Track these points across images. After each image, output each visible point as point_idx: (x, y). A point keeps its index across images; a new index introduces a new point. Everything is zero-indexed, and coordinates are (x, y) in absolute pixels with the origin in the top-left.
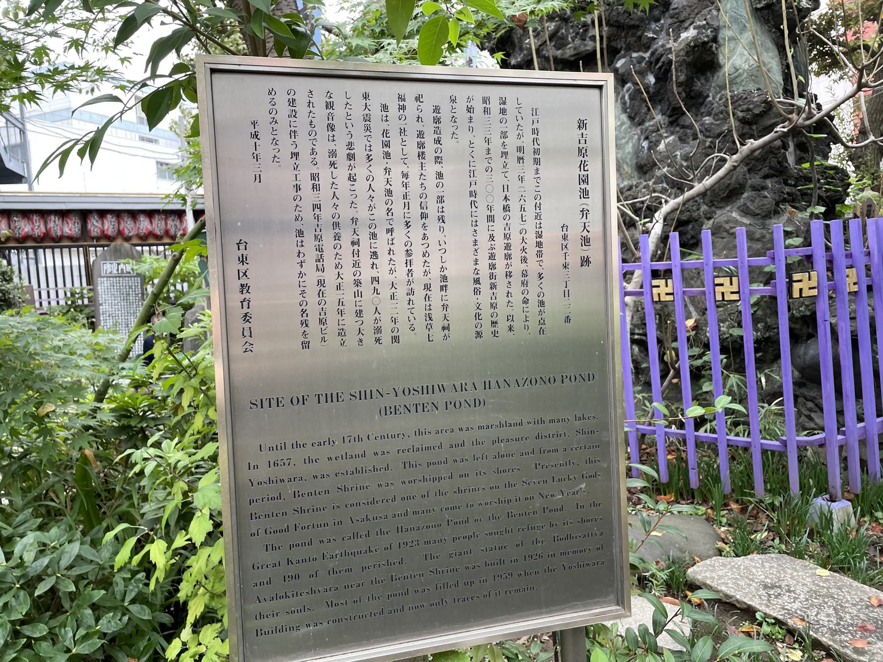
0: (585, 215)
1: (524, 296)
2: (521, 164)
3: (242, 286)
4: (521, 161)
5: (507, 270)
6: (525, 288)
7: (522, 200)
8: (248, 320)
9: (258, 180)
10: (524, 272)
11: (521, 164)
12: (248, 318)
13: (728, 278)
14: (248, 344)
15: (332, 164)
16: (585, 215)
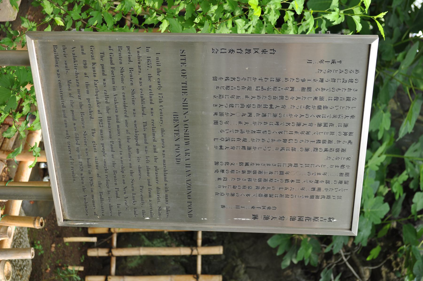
3: (250, 50)
8: (231, 52)
9: (309, 62)
12: (231, 52)
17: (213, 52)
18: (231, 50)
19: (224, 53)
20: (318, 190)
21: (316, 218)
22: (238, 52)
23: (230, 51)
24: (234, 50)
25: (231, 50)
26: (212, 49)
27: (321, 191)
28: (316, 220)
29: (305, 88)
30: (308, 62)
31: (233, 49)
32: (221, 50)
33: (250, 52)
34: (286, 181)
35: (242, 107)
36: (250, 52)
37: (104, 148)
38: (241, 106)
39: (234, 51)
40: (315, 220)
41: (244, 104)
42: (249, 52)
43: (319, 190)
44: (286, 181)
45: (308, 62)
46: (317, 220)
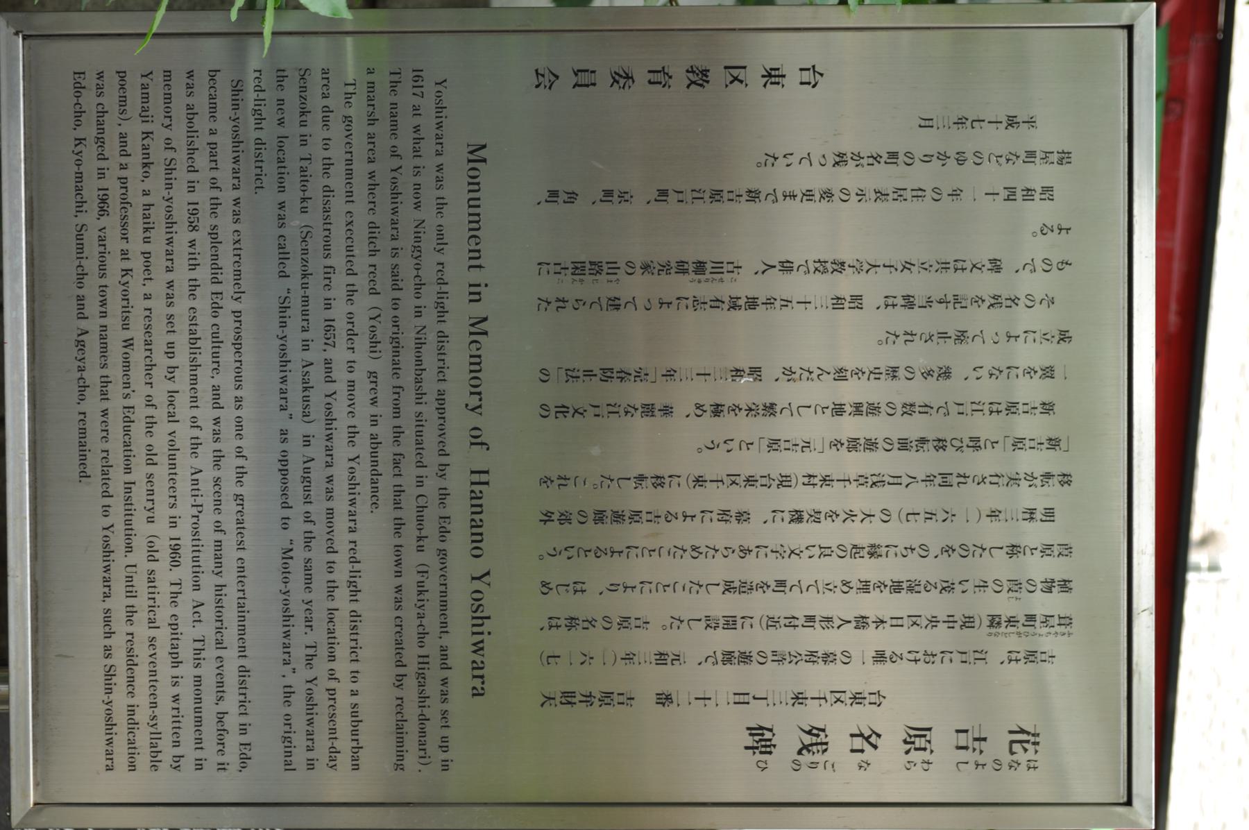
0: (584, 699)
1: (958, 549)
2: (1021, 516)
3: (705, 73)
4: (1027, 516)
5: (849, 155)
6: (1040, 586)
7: (945, 516)
8: (618, 82)
9: (923, 123)
10: (745, 516)
11: (1021, 516)
12: (622, 81)
13: (732, 79)
14: (553, 78)
15: (955, 194)
16: (584, 699)
17: (537, 86)
18: (621, 76)
19: (587, 86)
20: (1044, 518)
21: (916, 736)
22: (652, 81)
23: (617, 77)
24: (630, 75)
25: (621, 76)
26: (537, 71)
27: (1053, 521)
28: (917, 745)
29: (743, 371)
30: (920, 126)
31: (627, 71)
32: (576, 75)
33: (704, 78)
34: (860, 624)
35: (610, 271)
36: (704, 78)
37: (78, 401)
38: (609, 268)
39: (632, 78)
40: (913, 743)
41: (616, 263)
42: (701, 82)
43: (1048, 518)
44: (860, 624)
45: (920, 126)
46: (923, 746)
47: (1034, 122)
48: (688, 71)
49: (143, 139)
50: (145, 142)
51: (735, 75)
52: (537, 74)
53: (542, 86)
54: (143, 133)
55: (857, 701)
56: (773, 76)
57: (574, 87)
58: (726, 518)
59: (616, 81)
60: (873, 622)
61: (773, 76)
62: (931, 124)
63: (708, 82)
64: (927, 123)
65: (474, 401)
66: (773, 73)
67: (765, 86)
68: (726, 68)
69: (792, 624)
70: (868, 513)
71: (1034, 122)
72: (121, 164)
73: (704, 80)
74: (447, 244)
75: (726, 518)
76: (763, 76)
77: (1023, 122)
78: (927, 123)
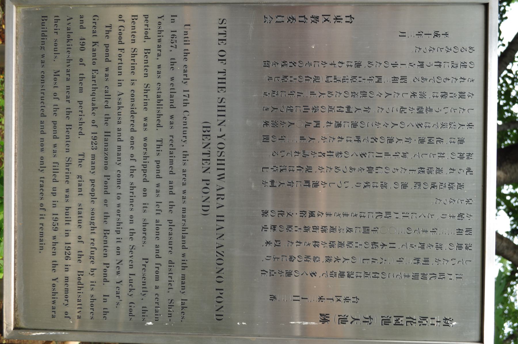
9: (401, 34)
13: (325, 20)
18: (291, 18)
19: (280, 22)
23: (290, 19)
25: (291, 18)
32: (277, 18)
33: (317, 20)
34: (374, 246)
36: (317, 20)
42: (315, 21)
44: (374, 246)
47: (448, 34)
48: (311, 17)
49: (93, 46)
50: (94, 47)
51: (327, 19)
52: (265, 17)
53: (267, 22)
54: (93, 42)
55: (338, 20)
56: (316, 19)
57: (276, 22)
58: (308, 259)
59: (289, 20)
60: (381, 245)
61: (316, 19)
62: (404, 35)
63: (318, 21)
64: (403, 34)
65: (66, 303)
66: (338, 18)
67: (335, 22)
68: (323, 15)
69: (341, 110)
70: (358, 108)
71: (448, 34)
72: (42, 61)
73: (317, 21)
74: (45, 167)
75: (308, 259)
76: (334, 19)
77: (442, 34)
78: (403, 34)
